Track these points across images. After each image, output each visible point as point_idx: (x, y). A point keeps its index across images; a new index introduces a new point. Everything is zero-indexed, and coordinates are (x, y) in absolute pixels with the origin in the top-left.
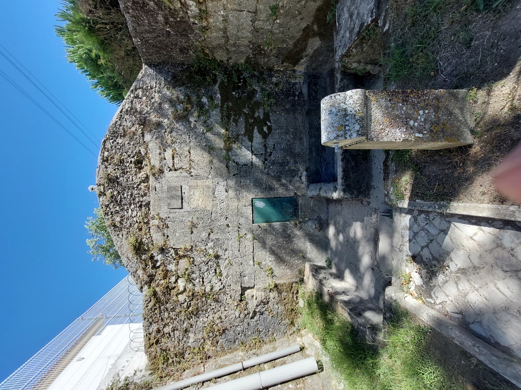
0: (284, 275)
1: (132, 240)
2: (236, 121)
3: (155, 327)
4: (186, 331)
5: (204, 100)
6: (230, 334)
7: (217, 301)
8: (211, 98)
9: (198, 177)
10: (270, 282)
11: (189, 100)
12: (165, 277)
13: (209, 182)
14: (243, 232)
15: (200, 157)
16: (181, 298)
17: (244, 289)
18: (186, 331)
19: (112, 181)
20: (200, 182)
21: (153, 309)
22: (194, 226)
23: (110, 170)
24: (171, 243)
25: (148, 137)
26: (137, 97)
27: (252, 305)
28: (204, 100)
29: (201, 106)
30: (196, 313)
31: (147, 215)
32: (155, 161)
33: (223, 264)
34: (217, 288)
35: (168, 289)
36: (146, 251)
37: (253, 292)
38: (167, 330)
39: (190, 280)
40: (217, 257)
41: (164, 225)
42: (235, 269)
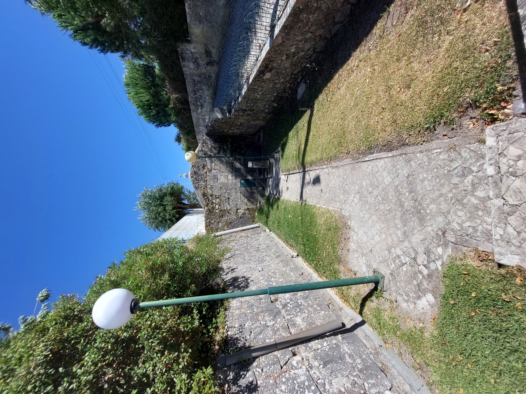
0: (251, 206)
1: (202, 192)
2: (235, 154)
3: (208, 220)
4: (219, 222)
5: (225, 147)
6: (233, 224)
7: (228, 213)
8: (227, 147)
9: (222, 172)
10: (246, 207)
11: (220, 148)
12: (212, 204)
13: (226, 174)
14: (237, 191)
15: (223, 168)
16: (217, 211)
17: (237, 209)
18: (219, 222)
19: (195, 173)
20: (223, 174)
21: (208, 214)
22: (221, 188)
23: (195, 169)
24: (214, 193)
25: (207, 159)
26: (203, 146)
27: (240, 214)
28: (225, 147)
29: (224, 149)
30: (222, 216)
31: (206, 184)
32: (209, 167)
33: (231, 201)
34: (229, 209)
35: (213, 208)
36: (206, 196)
37: (241, 210)
38: (212, 221)
39: (220, 205)
40: (229, 198)
41: (212, 188)
42: (235, 202)
